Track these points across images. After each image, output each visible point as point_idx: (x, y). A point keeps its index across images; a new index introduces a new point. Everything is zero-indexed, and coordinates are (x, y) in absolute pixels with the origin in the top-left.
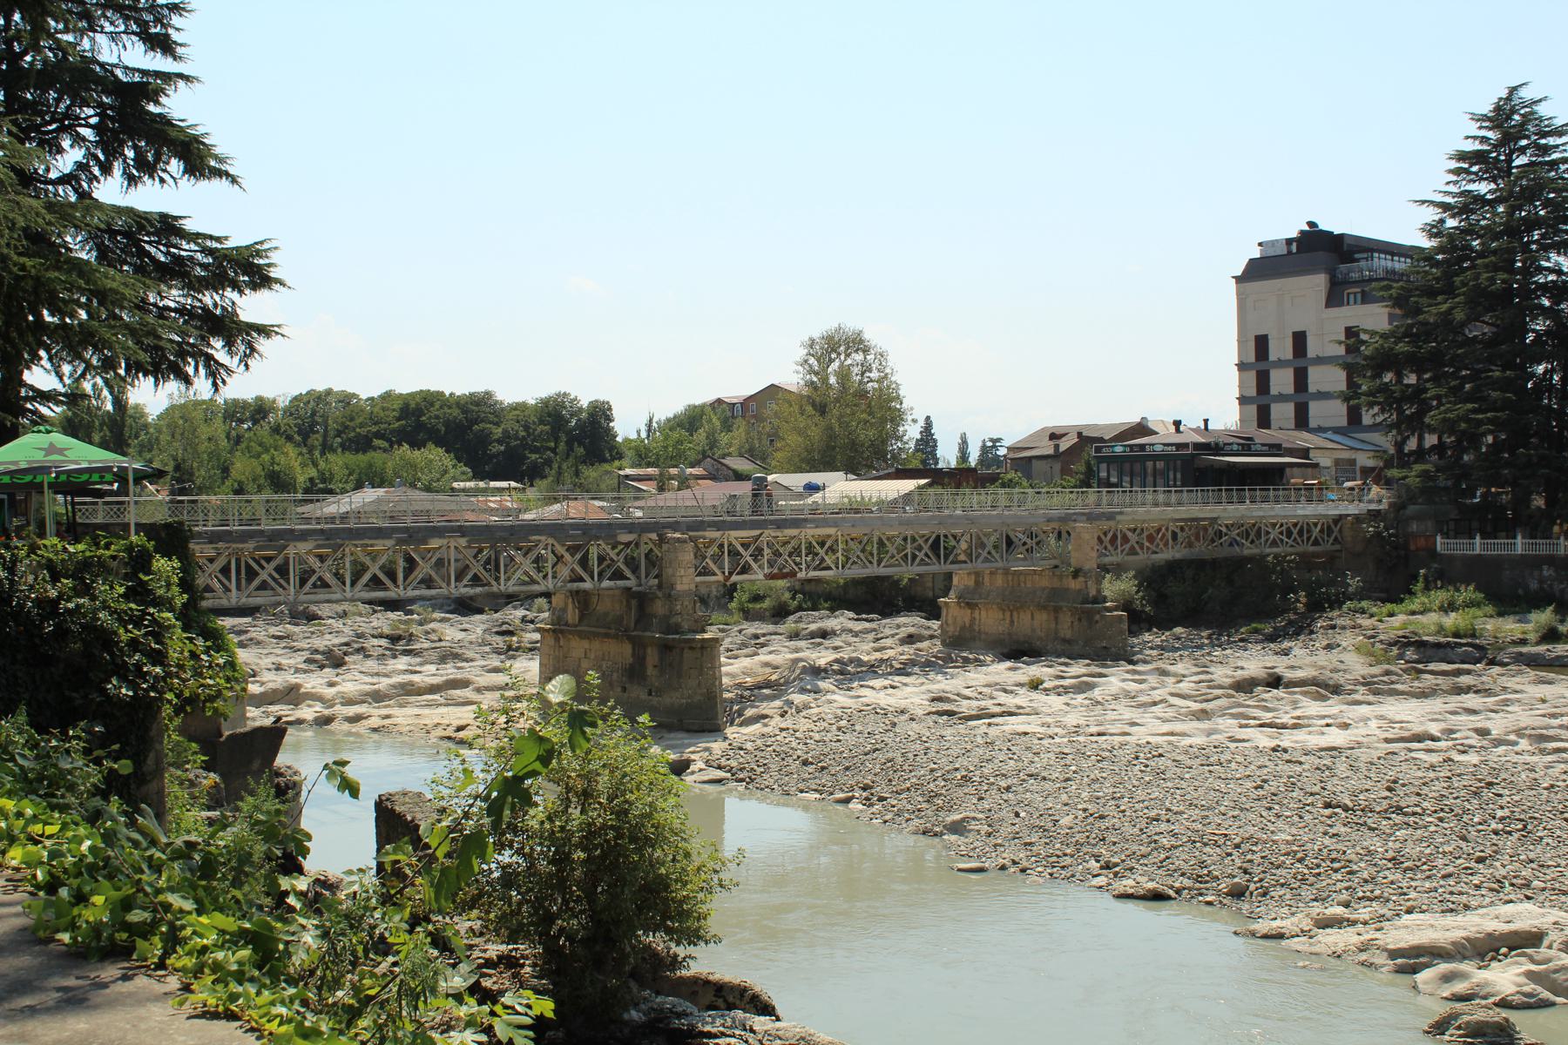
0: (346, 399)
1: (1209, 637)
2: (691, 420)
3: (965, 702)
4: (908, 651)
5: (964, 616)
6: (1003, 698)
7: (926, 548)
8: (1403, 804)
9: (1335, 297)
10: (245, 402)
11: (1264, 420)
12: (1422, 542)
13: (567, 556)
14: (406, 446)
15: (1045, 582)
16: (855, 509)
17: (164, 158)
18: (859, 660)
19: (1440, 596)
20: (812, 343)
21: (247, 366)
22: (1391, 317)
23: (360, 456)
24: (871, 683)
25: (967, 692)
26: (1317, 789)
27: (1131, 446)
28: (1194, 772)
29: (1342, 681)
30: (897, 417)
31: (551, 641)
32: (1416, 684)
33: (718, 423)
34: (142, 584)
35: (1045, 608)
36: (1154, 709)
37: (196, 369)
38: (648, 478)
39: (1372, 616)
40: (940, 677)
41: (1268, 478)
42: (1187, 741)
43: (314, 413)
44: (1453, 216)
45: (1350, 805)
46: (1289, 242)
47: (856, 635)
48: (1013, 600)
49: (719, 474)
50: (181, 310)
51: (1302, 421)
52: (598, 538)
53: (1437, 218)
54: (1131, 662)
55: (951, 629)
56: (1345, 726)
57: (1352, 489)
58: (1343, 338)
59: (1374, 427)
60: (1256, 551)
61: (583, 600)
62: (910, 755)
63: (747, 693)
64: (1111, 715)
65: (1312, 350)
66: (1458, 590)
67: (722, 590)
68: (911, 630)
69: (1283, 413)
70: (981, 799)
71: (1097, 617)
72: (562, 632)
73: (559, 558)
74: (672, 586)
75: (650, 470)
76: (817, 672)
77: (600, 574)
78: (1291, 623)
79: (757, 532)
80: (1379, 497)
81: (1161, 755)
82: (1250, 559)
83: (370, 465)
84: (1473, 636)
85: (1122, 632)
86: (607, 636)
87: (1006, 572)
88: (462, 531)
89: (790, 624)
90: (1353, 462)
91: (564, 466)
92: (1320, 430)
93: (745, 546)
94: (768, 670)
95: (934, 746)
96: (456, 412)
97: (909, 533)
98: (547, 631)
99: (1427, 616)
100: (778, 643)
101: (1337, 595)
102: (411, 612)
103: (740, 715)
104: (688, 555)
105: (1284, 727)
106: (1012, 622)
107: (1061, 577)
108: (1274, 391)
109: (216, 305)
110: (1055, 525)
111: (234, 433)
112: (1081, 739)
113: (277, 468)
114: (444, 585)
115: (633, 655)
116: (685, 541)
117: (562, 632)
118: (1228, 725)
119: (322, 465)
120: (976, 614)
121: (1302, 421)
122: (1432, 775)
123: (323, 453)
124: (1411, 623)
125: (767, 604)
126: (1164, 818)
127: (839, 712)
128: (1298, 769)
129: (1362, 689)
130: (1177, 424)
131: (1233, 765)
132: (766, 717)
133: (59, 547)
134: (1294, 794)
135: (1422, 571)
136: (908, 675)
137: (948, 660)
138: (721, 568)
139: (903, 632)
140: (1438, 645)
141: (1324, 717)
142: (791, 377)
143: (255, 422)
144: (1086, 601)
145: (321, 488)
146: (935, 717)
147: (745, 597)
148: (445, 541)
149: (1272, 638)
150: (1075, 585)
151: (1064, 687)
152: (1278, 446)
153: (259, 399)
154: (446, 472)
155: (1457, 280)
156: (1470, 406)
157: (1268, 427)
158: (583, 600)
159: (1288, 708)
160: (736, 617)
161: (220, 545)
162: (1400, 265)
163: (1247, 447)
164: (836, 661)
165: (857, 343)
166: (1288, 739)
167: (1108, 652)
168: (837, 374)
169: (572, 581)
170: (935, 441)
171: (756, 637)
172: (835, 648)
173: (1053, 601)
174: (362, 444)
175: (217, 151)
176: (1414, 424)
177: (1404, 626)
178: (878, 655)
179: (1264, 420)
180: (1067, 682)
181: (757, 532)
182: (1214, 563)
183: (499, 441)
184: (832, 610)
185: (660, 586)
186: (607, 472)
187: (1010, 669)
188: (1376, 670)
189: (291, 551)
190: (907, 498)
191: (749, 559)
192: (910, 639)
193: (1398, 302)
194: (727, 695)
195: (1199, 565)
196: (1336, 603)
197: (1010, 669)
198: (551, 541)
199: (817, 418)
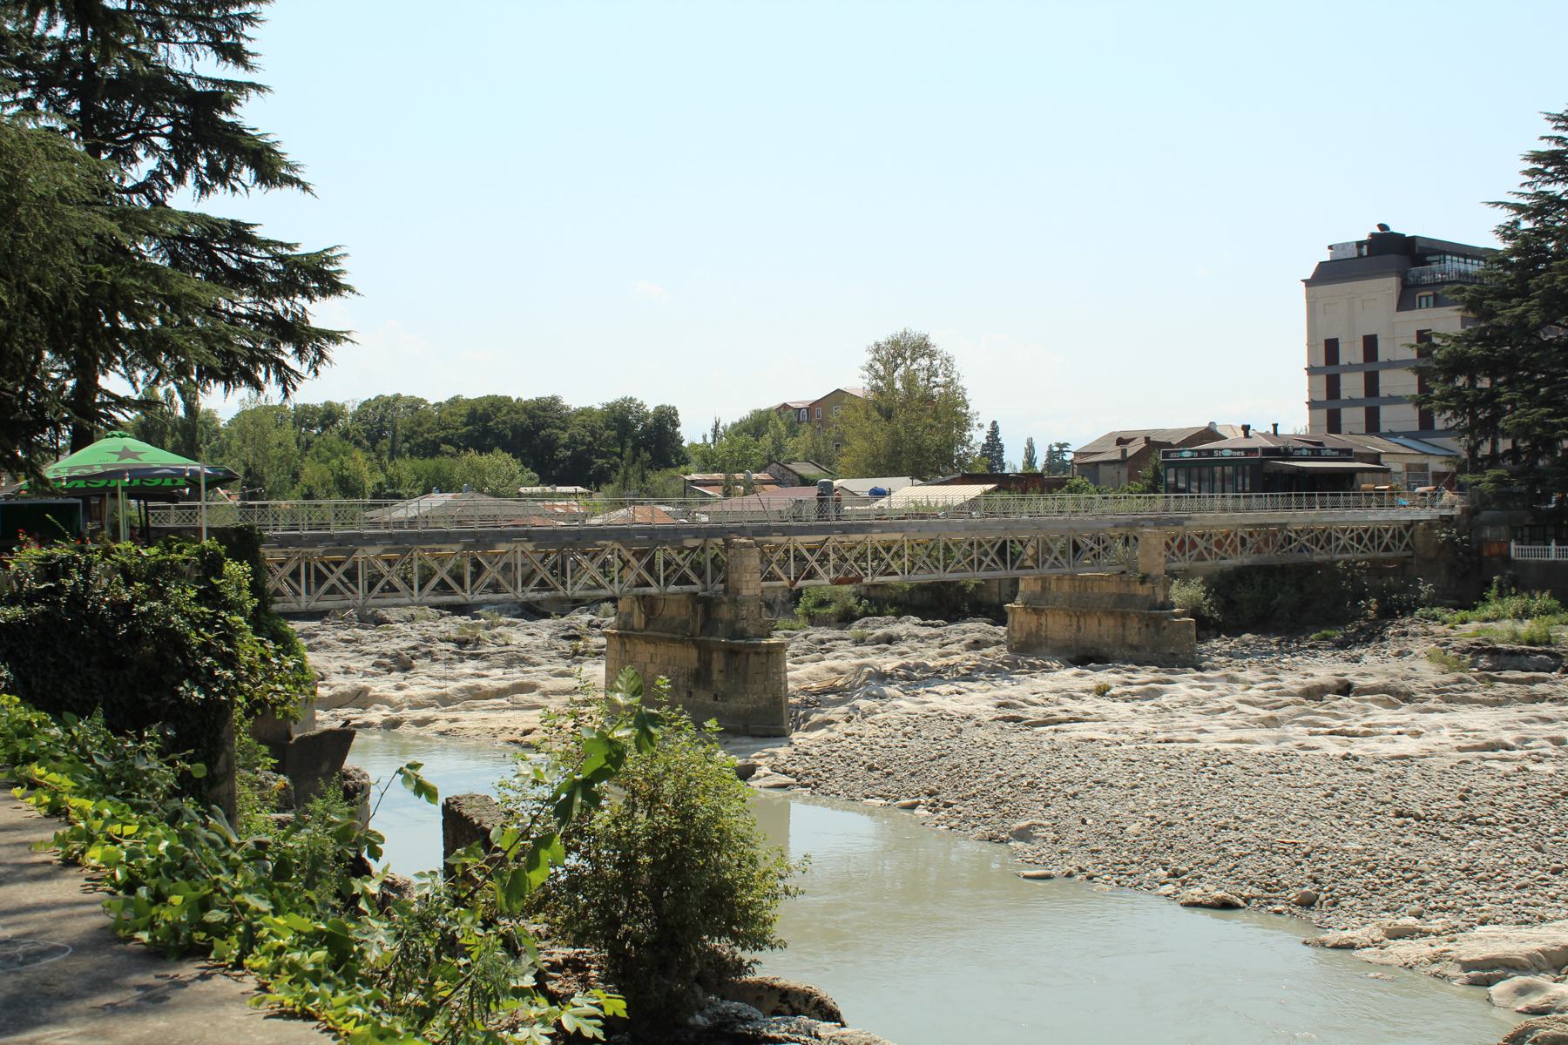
0: (415, 405)
1: (1278, 644)
2: (757, 425)
3: (1032, 708)
4: (974, 657)
5: (1031, 621)
6: (1069, 704)
8: (1476, 814)
9: (1406, 302)
10: (314, 407)
11: (1334, 425)
12: (1495, 549)
13: (633, 561)
15: (1112, 588)
16: (921, 514)
17: (236, 166)
19: (1514, 603)
20: (878, 348)
22: (1464, 322)
24: (936, 689)
25: (1034, 698)
26: (1388, 798)
28: (1262, 780)
29: (1414, 689)
30: (963, 422)
31: (616, 644)
32: (1490, 692)
34: (214, 587)
35: (1112, 613)
37: (267, 375)
38: (713, 483)
39: (1444, 623)
40: (1006, 683)
41: (1339, 483)
42: (1256, 749)
43: (382, 419)
44: (1528, 218)
45: (1422, 814)
46: (1360, 244)
47: (922, 640)
48: (1080, 606)
50: (252, 317)
51: (1372, 426)
52: (664, 543)
54: (1199, 669)
55: (1017, 635)
56: (1417, 734)
57: (1424, 494)
58: (1414, 342)
59: (1447, 432)
60: (1326, 557)
62: (976, 762)
64: (1179, 722)
66: (1532, 597)
68: (978, 636)
69: (1353, 417)
71: (1165, 623)
72: (628, 636)
74: (738, 592)
76: (883, 677)
77: (666, 579)
78: (1361, 630)
79: (821, 538)
80: (1451, 502)
81: (1229, 763)
82: (1320, 565)
83: (438, 470)
84: (1549, 643)
85: (1190, 639)
86: (672, 640)
87: (1073, 577)
88: (529, 536)
89: (855, 629)
90: (1425, 467)
91: (631, 471)
92: (1391, 434)
93: (811, 551)
94: (834, 675)
95: (1000, 752)
96: (523, 417)
97: (975, 538)
98: (614, 635)
99: (1501, 623)
100: (843, 648)
103: (806, 720)
104: (753, 560)
105: (1354, 734)
106: (1079, 628)
107: (1128, 583)
108: (1344, 395)
109: (286, 311)
110: (1123, 530)
114: (511, 589)
115: (699, 659)
116: (751, 547)
117: (628, 636)
118: (1297, 733)
119: (391, 469)
120: (1043, 620)
121: (1372, 426)
122: (1506, 784)
123: (391, 458)
124: (1484, 630)
126: (1232, 826)
127: (905, 718)
128: (1369, 777)
129: (1434, 697)
130: (1246, 428)
132: (832, 722)
134: (1365, 803)
136: (974, 680)
137: (1014, 666)
138: (787, 573)
139: (970, 638)
140: (1512, 653)
141: (1395, 725)
142: (857, 383)
143: (325, 427)
144: (1153, 607)
145: (389, 493)
146: (1001, 723)
148: (512, 546)
149: (1342, 645)
150: (1142, 590)
153: (329, 404)
154: (513, 477)
155: (1532, 282)
156: (1545, 410)
157: (1338, 431)
160: (802, 622)
161: (290, 549)
162: (1473, 267)
163: (1316, 452)
164: (902, 666)
165: (922, 348)
166: (1358, 747)
167: (1174, 657)
169: (638, 586)
170: (1001, 446)
171: (822, 642)
172: (901, 654)
173: (1121, 606)
174: (430, 449)
175: (288, 158)
176: (1489, 429)
177: (1477, 633)
178: (944, 661)
179: (1334, 425)
181: (821, 538)
182: (1283, 569)
183: (566, 447)
184: (898, 615)
185: (726, 591)
186: (674, 477)
187: (1077, 675)
188: (1449, 678)
189: (360, 555)
191: (815, 564)
192: (977, 645)
194: (792, 700)
195: (1268, 571)
196: (1408, 610)
197: (1077, 675)
198: (617, 546)
199: (883, 423)
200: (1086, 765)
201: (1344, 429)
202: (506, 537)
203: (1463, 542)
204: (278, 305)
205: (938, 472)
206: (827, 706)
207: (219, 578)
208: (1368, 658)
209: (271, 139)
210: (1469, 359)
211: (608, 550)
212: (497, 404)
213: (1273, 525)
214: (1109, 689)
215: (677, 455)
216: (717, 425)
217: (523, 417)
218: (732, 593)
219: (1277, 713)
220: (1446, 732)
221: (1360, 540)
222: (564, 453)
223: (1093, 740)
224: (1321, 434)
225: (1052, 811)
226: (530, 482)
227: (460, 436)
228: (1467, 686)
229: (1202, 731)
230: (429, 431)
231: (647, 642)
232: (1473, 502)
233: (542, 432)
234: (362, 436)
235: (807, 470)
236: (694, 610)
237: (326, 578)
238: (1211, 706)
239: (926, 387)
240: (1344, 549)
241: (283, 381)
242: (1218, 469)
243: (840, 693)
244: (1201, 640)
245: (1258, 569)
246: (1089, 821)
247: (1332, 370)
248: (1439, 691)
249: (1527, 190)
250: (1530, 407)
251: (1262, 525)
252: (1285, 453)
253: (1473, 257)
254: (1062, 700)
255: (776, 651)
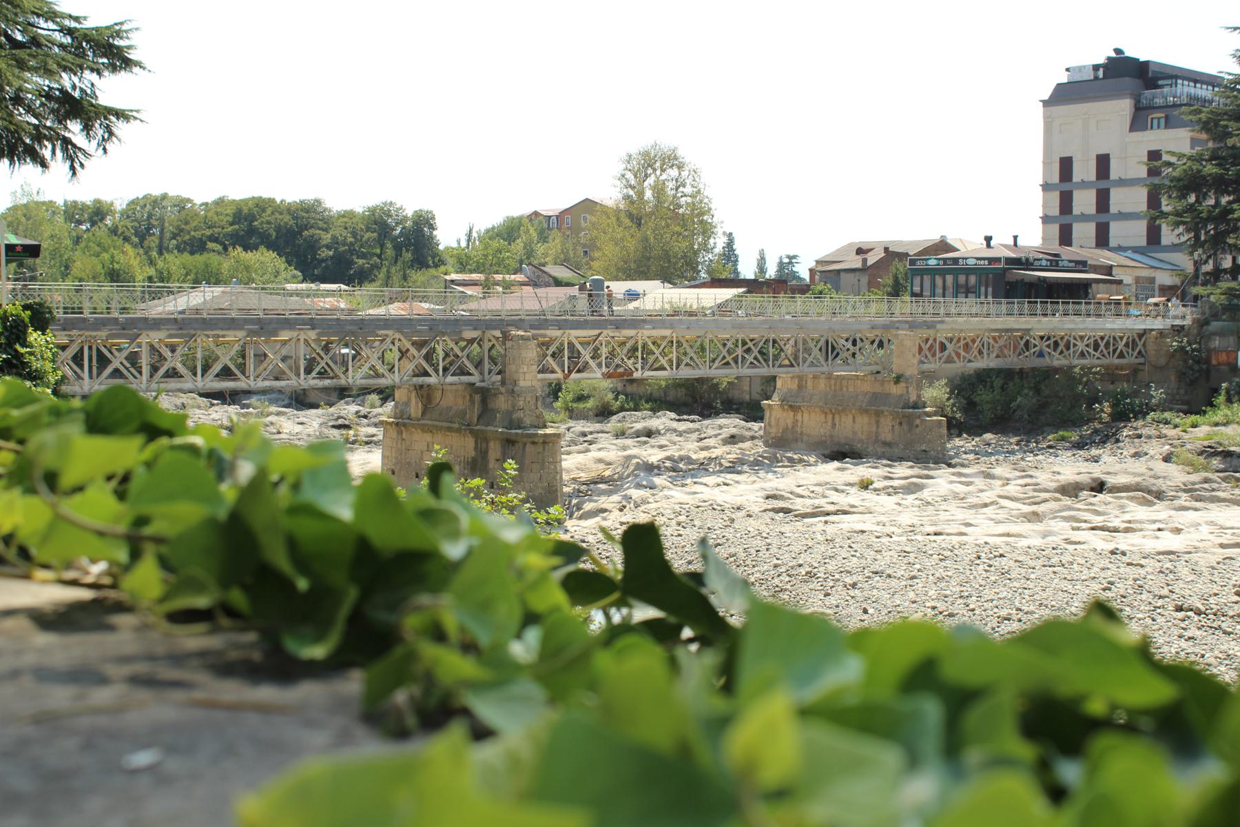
0: (181, 204)
2: (510, 230)
3: (799, 500)
4: (733, 452)
5: (787, 418)
6: (834, 496)
7: (755, 352)
9: (1139, 121)
10: (83, 204)
11: (1066, 237)
13: (413, 351)
14: (240, 249)
15: (867, 387)
16: (676, 313)
18: (689, 458)
21: (105, 150)
22: (1194, 142)
23: (197, 257)
24: (704, 480)
25: (799, 491)
26: (1165, 592)
27: (945, 260)
28: (1038, 573)
29: (1164, 488)
30: (707, 230)
31: (393, 433)
33: (535, 235)
34: (18, 356)
35: (866, 411)
36: (985, 510)
37: (54, 152)
38: (474, 283)
39: (1176, 426)
40: (770, 475)
41: (1076, 291)
42: (1024, 543)
43: (150, 216)
45: (1203, 609)
46: (1096, 68)
47: (680, 434)
48: (835, 405)
51: (1102, 239)
52: (443, 334)
54: (950, 465)
55: (773, 430)
56: (1178, 531)
57: (1156, 305)
58: (1145, 159)
59: (1175, 248)
60: (1064, 362)
61: (425, 393)
62: (753, 551)
64: (943, 516)
65: (1115, 172)
68: (734, 431)
69: (1084, 232)
70: (827, 595)
71: (918, 422)
72: (405, 425)
73: (403, 354)
74: (515, 383)
75: (475, 276)
76: (650, 468)
77: (445, 369)
78: (1096, 431)
79: (597, 332)
80: (1181, 314)
81: (1002, 556)
82: (1056, 370)
85: (941, 437)
86: (450, 429)
87: (829, 377)
88: (312, 324)
89: (613, 423)
90: (1152, 280)
91: (393, 270)
92: (1120, 249)
94: (602, 466)
95: (775, 542)
96: (287, 218)
97: (740, 336)
100: (605, 440)
101: (1140, 406)
102: (248, 406)
103: (579, 509)
105: (1116, 530)
106: (834, 425)
107: (882, 383)
108: (1076, 210)
109: (74, 87)
111: (74, 234)
112: (919, 538)
113: (116, 266)
114: (293, 376)
115: (476, 448)
116: (528, 339)
117: (405, 425)
118: (1061, 528)
119: (160, 264)
120: (799, 417)
121: (1102, 239)
123: (160, 253)
124: (1215, 434)
126: (1015, 617)
127: (677, 507)
128: (1142, 572)
130: (988, 239)
132: (605, 511)
134: (1144, 597)
136: (739, 473)
137: (774, 460)
139: (726, 433)
141: (1155, 522)
142: (609, 193)
143: (93, 224)
144: (907, 406)
145: (160, 285)
146: (771, 514)
147: (570, 397)
148: (294, 334)
149: (1079, 446)
150: (896, 390)
152: (1084, 263)
153: (97, 201)
157: (1070, 245)
158: (425, 393)
159: (1117, 512)
160: (562, 416)
161: (75, 332)
162: (1204, 92)
163: (1054, 262)
164: (668, 458)
165: (671, 160)
170: (736, 256)
172: (661, 447)
173: (875, 405)
174: (197, 246)
176: (1217, 243)
177: (1209, 436)
178: (704, 454)
179: (1066, 237)
180: (896, 483)
181: (597, 332)
183: (328, 247)
185: (503, 383)
187: (839, 469)
188: (1195, 477)
189: (144, 339)
190: (722, 308)
192: (733, 439)
193: (1205, 126)
194: (566, 489)
195: (1008, 374)
196: (1141, 413)
197: (839, 469)
198: (397, 336)
199: (634, 229)
200: (862, 556)
201: (1074, 242)
202: (288, 324)
203: (1193, 350)
204: (67, 80)
206: (599, 495)
207: (24, 345)
208: (1106, 458)
210: (1204, 177)
211: (389, 340)
212: (262, 205)
213: (1017, 330)
214: (872, 483)
215: (433, 258)
216: (471, 230)
217: (287, 218)
219: (1040, 509)
220: (1205, 529)
222: (326, 253)
223: (863, 532)
224: (1055, 247)
225: (832, 600)
228: (1215, 486)
229: (968, 525)
231: (423, 431)
232: (1203, 313)
233: (305, 233)
235: (562, 273)
236: (472, 401)
238: (974, 500)
239: (675, 196)
240: (1082, 355)
241: (71, 159)
242: (949, 279)
243: (612, 483)
244: (950, 436)
245: (999, 372)
246: (871, 611)
247: (1066, 187)
248: (1188, 490)
251: (1007, 330)
253: (1202, 83)
254: (828, 493)
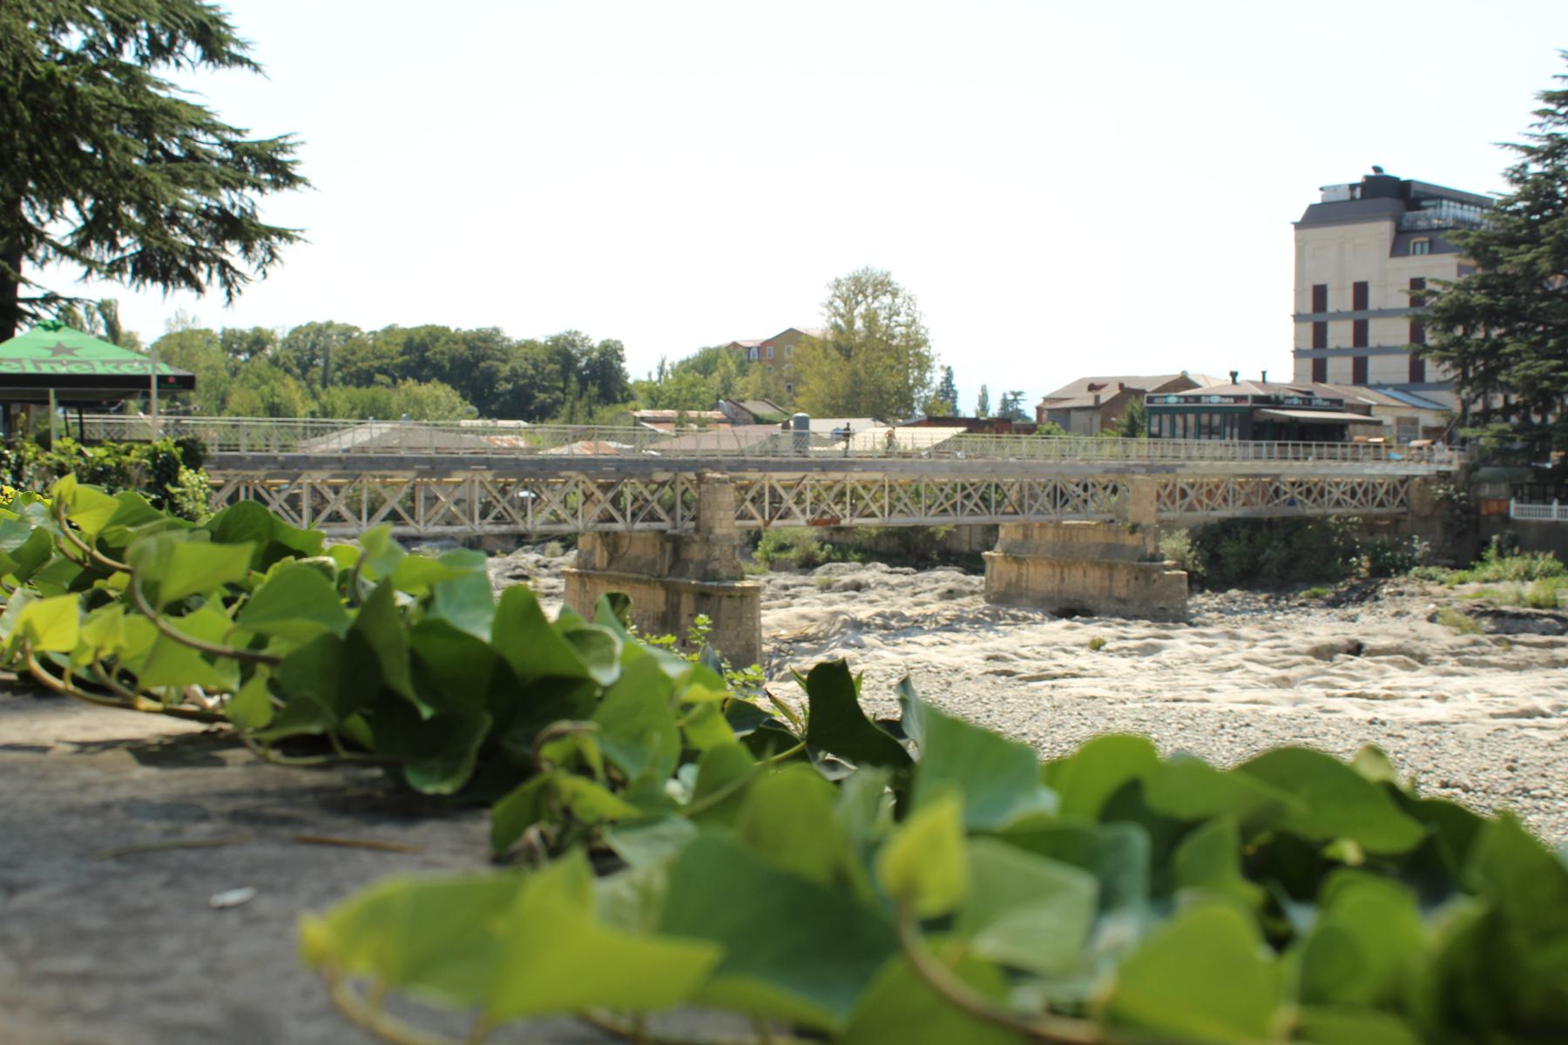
0: (347, 332)
1: (1266, 601)
2: (706, 363)
3: (1023, 662)
6: (1063, 659)
8: (1530, 786)
9: (1401, 244)
11: (1319, 374)
12: (1494, 507)
13: (598, 494)
15: (1099, 538)
17: (179, 43)
19: (1515, 564)
20: (838, 284)
22: (1461, 269)
23: (363, 390)
24: (918, 639)
25: (1023, 651)
26: (1429, 766)
27: (1186, 398)
29: (1428, 651)
30: (924, 364)
31: (576, 585)
32: (1509, 656)
33: (733, 368)
36: (1230, 674)
37: (210, 276)
38: (666, 421)
39: (1441, 583)
40: (991, 634)
41: (1331, 433)
42: (1273, 711)
43: (314, 345)
44: (1537, 161)
45: (1470, 784)
46: (1353, 187)
47: (892, 588)
49: (737, 417)
50: (197, 212)
51: (1360, 376)
52: (631, 476)
53: (1519, 162)
54: (1191, 625)
55: (996, 586)
56: (1443, 699)
57: (1420, 448)
58: (1407, 287)
59: (1440, 385)
61: (611, 541)
63: (785, 647)
64: (1183, 680)
65: (1374, 302)
66: (1535, 558)
67: (746, 539)
68: (951, 585)
69: (1339, 368)
71: (1155, 576)
72: (588, 576)
73: (588, 497)
74: (710, 530)
75: (668, 413)
76: (859, 626)
77: (634, 515)
79: (799, 475)
80: (1448, 459)
82: (1309, 520)
83: (374, 400)
84: (1555, 607)
85: (1181, 593)
86: (638, 581)
87: (1058, 525)
88: (489, 464)
90: (1415, 421)
91: (578, 405)
93: (787, 488)
94: (805, 623)
95: (996, 708)
96: (462, 348)
98: (573, 574)
99: (1504, 583)
100: (809, 594)
101: (1403, 559)
103: (780, 670)
104: (728, 497)
105: (1374, 697)
106: (1062, 579)
107: (1117, 532)
108: (1332, 343)
109: (233, 205)
110: (1112, 477)
112: (1157, 705)
113: (277, 400)
115: (667, 601)
117: (588, 576)
119: (324, 398)
120: (1024, 570)
121: (1360, 376)
122: (1552, 755)
123: (324, 386)
124: (1486, 592)
125: (793, 554)
127: (888, 669)
128: (1403, 743)
129: (1451, 660)
131: (1329, 737)
133: (74, 449)
135: (1495, 538)
136: (957, 631)
137: (996, 618)
138: (762, 512)
140: (1517, 616)
141: (1417, 688)
142: (815, 321)
143: (253, 353)
144: (1143, 558)
146: (992, 677)
148: (469, 475)
149: (1334, 603)
150: (1131, 541)
151: (1129, 649)
154: (453, 409)
155: (1543, 229)
156: (1553, 363)
158: (611, 541)
159: (1376, 678)
161: (230, 472)
162: (1471, 214)
163: (1307, 402)
164: (879, 615)
165: (883, 286)
166: (1383, 711)
167: (1170, 615)
168: (864, 317)
169: (601, 521)
170: (955, 392)
171: (786, 588)
172: (871, 602)
173: (1108, 557)
175: (237, 34)
176: (1487, 381)
177: (1478, 595)
178: (918, 610)
179: (1319, 374)
180: (1131, 644)
182: (1270, 523)
183: (507, 380)
184: (864, 561)
185: (697, 530)
186: (623, 414)
187: (1068, 628)
192: (950, 594)
193: (1474, 252)
194: (765, 648)
195: (1255, 524)
196: (1403, 568)
198: (582, 477)
199: (842, 362)
203: (1461, 499)
204: (226, 197)
205: (897, 415)
209: (222, 11)
211: (572, 483)
212: (435, 334)
214: (1104, 643)
218: (703, 531)
220: (1473, 697)
221: (1353, 494)
223: (1094, 698)
224: (1308, 384)
226: (469, 415)
227: (396, 366)
228: (1485, 649)
229: (1211, 691)
230: (363, 360)
232: (1472, 458)
233: (482, 365)
234: (292, 364)
237: (286, 501)
238: (1216, 663)
240: (1338, 503)
241: (227, 283)
244: (1191, 592)
245: (1245, 522)
249: (1536, 131)
250: (1537, 359)
252: (1277, 402)
253: (1470, 204)
254: (1055, 654)
255: (749, 597)
